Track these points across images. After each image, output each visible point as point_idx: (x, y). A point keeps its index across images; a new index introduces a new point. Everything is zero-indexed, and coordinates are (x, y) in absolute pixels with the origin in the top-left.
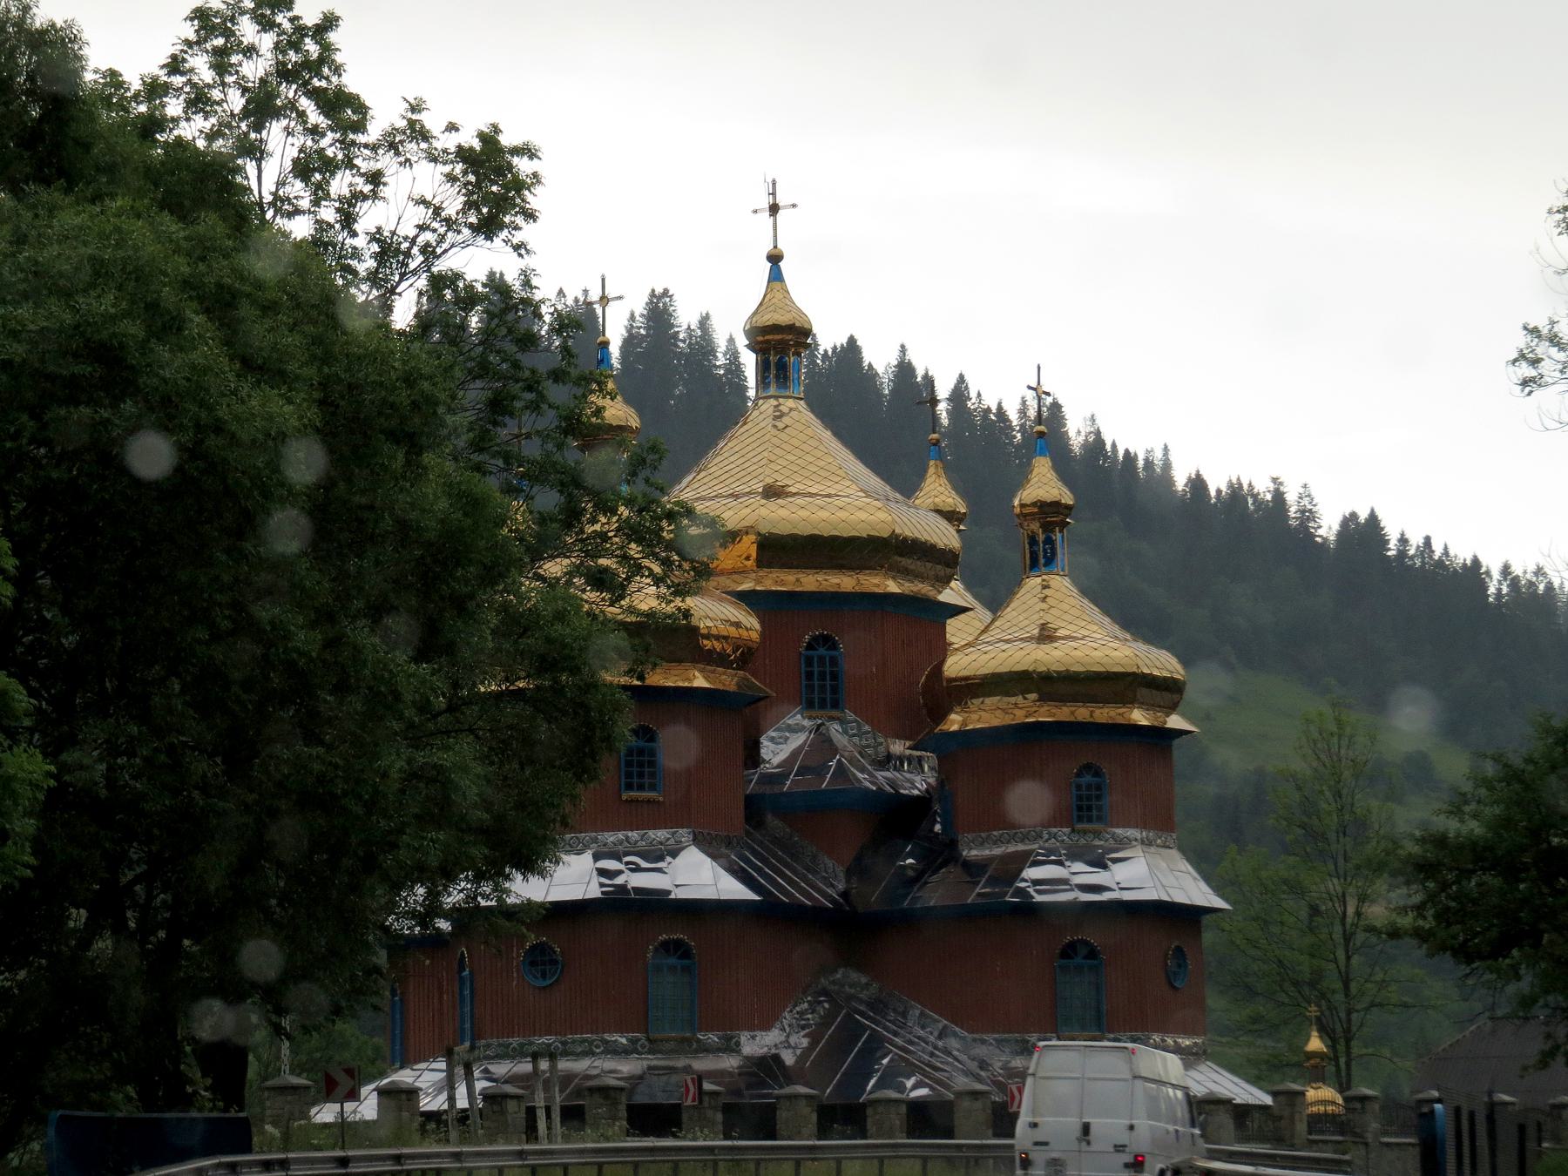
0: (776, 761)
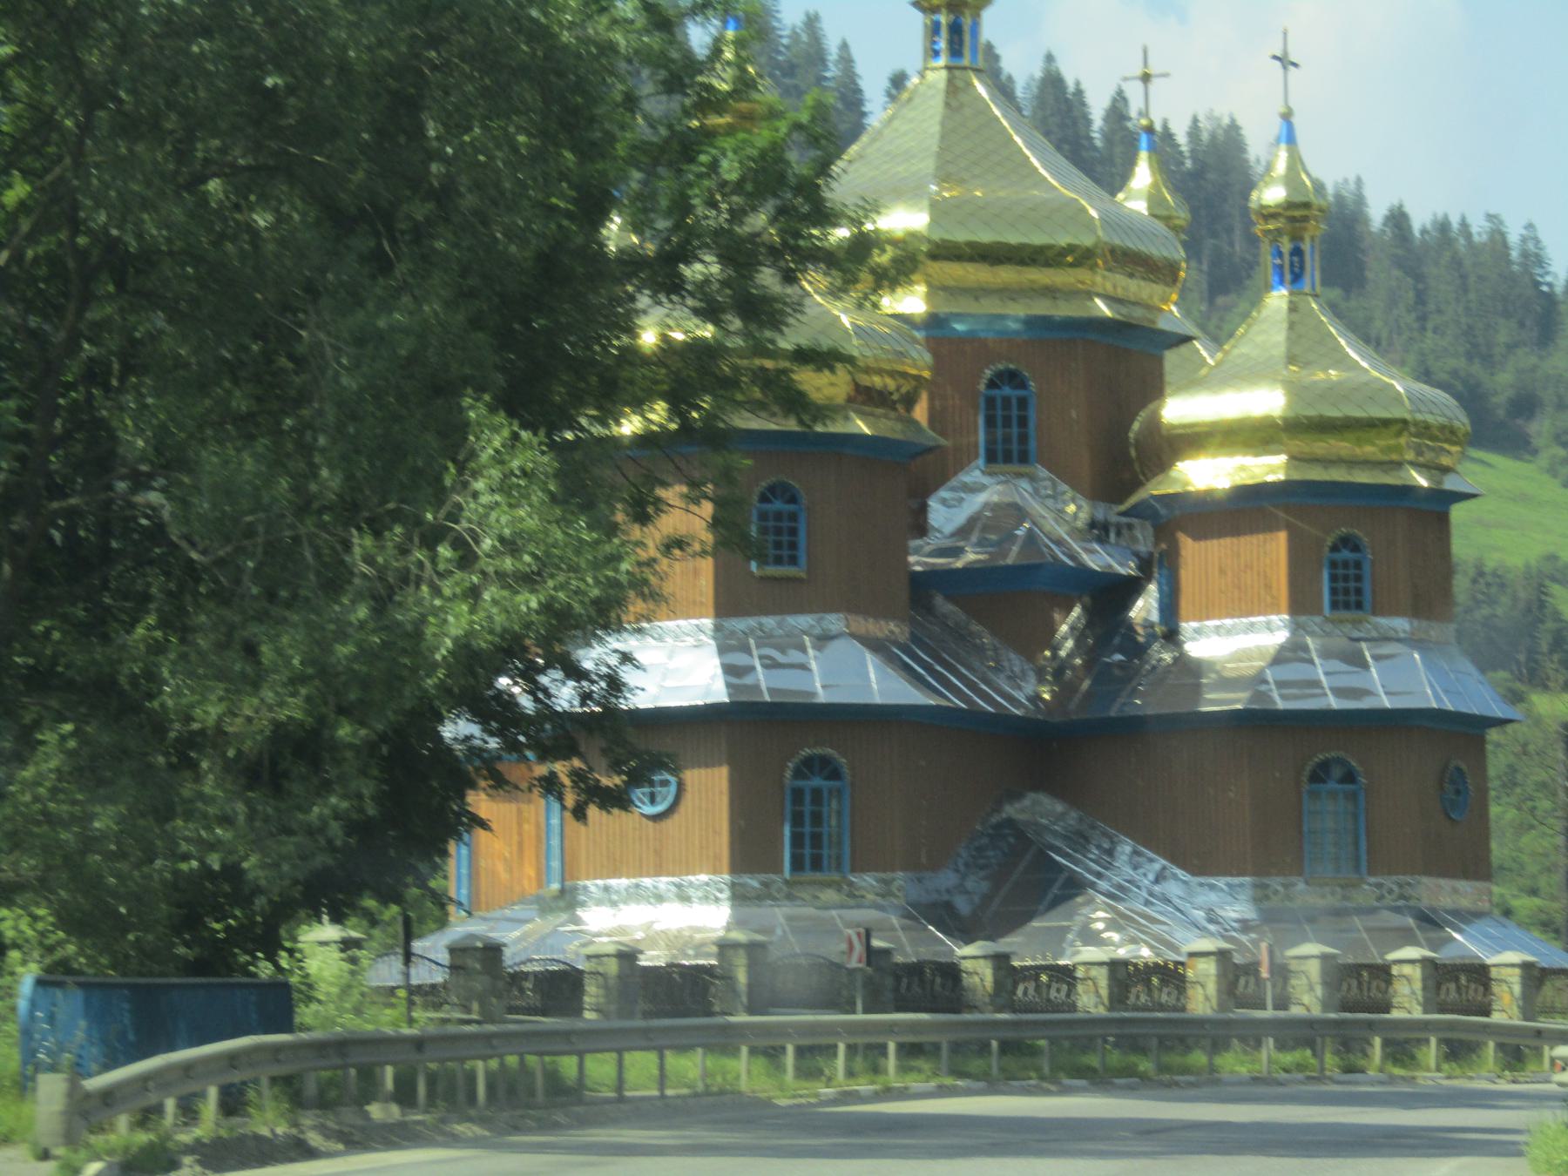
0: (949, 529)
